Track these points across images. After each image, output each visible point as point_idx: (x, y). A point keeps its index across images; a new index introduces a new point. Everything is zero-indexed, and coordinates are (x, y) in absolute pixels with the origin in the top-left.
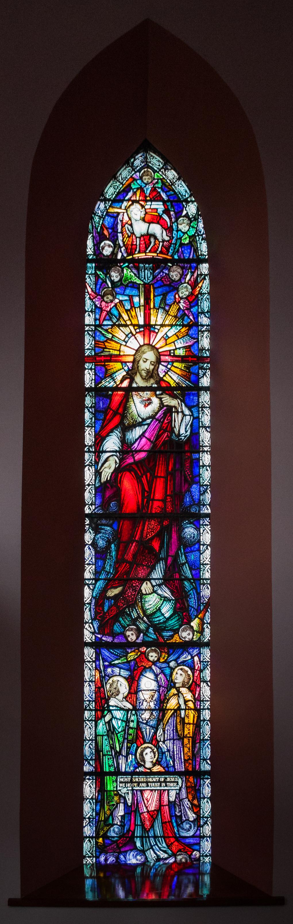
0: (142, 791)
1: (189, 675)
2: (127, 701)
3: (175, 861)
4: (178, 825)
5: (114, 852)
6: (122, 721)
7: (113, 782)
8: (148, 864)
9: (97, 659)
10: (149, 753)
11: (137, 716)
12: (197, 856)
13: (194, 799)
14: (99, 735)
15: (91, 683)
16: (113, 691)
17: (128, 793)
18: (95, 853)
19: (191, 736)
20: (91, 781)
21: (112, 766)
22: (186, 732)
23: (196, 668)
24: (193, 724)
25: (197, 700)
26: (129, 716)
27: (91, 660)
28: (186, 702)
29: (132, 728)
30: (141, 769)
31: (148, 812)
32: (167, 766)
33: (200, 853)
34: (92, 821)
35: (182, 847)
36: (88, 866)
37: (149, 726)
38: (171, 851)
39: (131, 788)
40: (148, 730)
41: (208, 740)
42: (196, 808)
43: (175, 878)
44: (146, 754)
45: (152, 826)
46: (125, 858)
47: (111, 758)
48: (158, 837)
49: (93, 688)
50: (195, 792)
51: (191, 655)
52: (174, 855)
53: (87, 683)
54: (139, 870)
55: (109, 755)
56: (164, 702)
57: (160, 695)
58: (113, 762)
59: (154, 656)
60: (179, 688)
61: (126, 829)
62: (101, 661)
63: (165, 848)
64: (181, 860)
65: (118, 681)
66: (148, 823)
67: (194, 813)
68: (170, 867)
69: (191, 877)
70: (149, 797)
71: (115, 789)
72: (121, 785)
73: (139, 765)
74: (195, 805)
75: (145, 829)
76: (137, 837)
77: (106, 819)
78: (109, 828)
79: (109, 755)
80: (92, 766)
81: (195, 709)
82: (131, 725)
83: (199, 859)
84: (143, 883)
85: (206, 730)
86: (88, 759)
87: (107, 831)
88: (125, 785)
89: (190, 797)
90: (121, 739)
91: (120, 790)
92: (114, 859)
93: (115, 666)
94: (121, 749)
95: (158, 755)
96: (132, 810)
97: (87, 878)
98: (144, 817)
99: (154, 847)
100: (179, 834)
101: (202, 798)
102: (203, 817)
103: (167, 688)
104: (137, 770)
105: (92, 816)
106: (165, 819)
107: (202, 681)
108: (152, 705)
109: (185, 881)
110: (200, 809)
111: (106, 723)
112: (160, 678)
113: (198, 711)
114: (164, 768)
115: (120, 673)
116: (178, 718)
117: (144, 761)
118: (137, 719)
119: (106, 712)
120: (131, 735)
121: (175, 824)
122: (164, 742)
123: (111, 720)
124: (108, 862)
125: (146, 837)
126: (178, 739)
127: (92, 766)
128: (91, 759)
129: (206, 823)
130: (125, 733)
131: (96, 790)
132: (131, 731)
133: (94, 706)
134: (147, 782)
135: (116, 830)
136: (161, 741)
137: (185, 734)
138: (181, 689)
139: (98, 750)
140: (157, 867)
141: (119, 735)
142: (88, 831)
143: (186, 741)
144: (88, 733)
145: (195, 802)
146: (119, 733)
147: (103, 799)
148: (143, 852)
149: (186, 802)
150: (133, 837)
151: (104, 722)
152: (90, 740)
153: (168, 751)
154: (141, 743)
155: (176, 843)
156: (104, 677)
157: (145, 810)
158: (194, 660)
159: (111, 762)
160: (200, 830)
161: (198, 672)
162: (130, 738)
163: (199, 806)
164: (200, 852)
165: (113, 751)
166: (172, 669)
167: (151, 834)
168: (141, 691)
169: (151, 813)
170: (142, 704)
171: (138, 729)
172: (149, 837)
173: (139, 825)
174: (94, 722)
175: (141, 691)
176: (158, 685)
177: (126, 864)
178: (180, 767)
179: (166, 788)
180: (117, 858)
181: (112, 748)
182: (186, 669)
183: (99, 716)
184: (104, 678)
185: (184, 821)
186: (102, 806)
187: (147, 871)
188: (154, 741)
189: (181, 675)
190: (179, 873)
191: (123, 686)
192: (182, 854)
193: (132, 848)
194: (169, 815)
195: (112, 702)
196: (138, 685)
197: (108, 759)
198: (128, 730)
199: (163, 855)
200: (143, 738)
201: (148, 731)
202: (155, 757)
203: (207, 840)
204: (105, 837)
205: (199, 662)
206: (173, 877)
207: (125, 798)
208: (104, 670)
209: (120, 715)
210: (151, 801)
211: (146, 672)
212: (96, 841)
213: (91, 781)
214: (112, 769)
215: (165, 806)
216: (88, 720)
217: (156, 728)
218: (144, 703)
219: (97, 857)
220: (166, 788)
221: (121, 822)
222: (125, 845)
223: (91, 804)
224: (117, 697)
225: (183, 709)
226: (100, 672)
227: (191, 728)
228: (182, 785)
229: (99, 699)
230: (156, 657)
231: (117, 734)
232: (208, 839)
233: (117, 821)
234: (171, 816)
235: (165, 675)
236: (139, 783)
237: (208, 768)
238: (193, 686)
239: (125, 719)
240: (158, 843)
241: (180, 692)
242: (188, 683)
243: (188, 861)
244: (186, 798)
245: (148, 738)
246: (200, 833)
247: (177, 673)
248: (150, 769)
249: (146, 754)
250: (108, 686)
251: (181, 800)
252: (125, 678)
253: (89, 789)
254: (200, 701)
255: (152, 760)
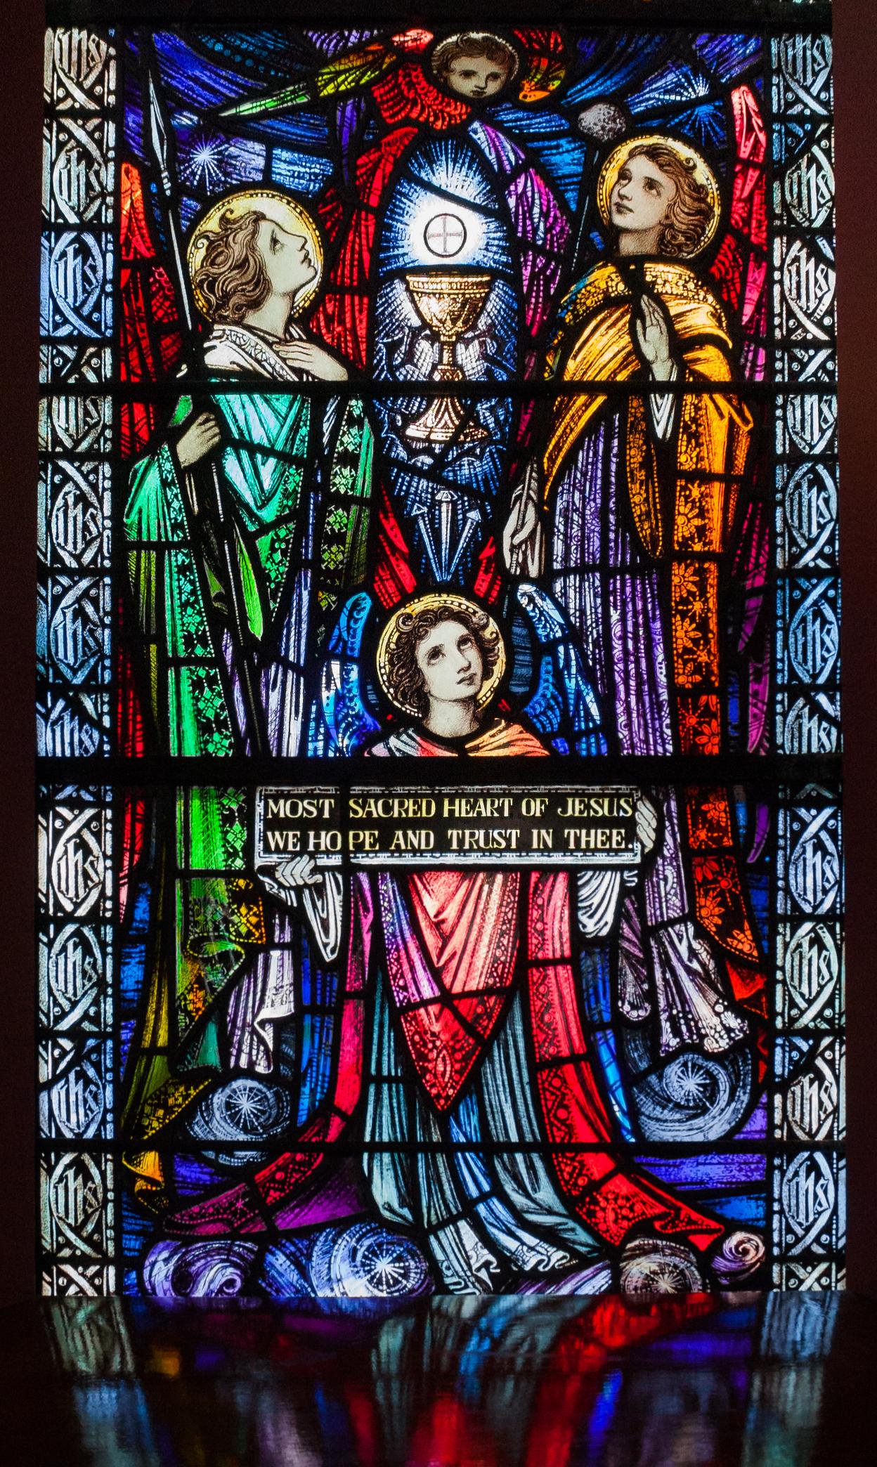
0: (406, 878)
1: (699, 190)
2: (314, 338)
3: (616, 1288)
4: (632, 1080)
5: (235, 1236)
6: (285, 458)
7: (228, 820)
8: (449, 1304)
9: (131, 96)
10: (450, 648)
11: (376, 428)
12: (751, 1258)
13: (731, 922)
14: (140, 545)
15: (89, 239)
16: (229, 279)
17: (319, 889)
18: (117, 1240)
19: (716, 546)
20: (89, 813)
21: (221, 725)
22: (684, 526)
23: (745, 151)
24: (726, 478)
25: (750, 333)
26: (327, 427)
27: (92, 106)
28: (681, 345)
29: (345, 502)
30: (403, 744)
31: (446, 999)
32: (566, 729)
33: (769, 1243)
34: (97, 1049)
35: (659, 1209)
36: (81, 1316)
37: (452, 485)
38: (588, 1229)
39: (336, 860)
40: (445, 512)
41: (818, 574)
42: (747, 979)
43: (608, 1392)
44: (436, 653)
45: (472, 1085)
46: (304, 1272)
47: (212, 681)
48: (511, 1148)
49: (106, 265)
50: (741, 890)
51: (713, 81)
52: (611, 1255)
53: (68, 237)
54: (391, 1340)
55: (200, 662)
56: (542, 349)
57: (523, 300)
58: (229, 704)
59: (483, 74)
60: (640, 260)
61: (305, 1102)
62: (155, 109)
63: (550, 1212)
64: (650, 1279)
65: (259, 217)
66: (442, 1066)
67: (735, 1007)
68: (577, 1324)
69: (704, 1383)
70: (450, 913)
71: (239, 863)
72: (275, 839)
73: (392, 722)
74: (739, 961)
75: (429, 1102)
76: (377, 1148)
77: (182, 1047)
78: (205, 1096)
79: (200, 662)
80: (97, 724)
81: (738, 389)
82: (342, 480)
83: (761, 1278)
84: (420, 1413)
85: (814, 514)
86: (67, 684)
87: (189, 1114)
88: (304, 841)
89: (711, 913)
90: (276, 568)
91: (269, 871)
92: (230, 1272)
93: (243, 129)
94: (275, 626)
95: (510, 664)
96: (345, 989)
97: (85, 1382)
98: (422, 1031)
99: (481, 1209)
100: (637, 1130)
101: (784, 919)
102: (788, 1032)
103: (564, 260)
104: (379, 750)
105: (95, 1020)
106: (554, 1040)
107: (780, 232)
108: (471, 360)
109: (668, 1405)
110: (772, 982)
111: (181, 472)
112: (521, 198)
113: (757, 399)
114: (545, 739)
115: (267, 171)
116: (636, 440)
117: (423, 699)
118: (379, 443)
119: (183, 408)
120: (338, 538)
121: (612, 1074)
122: (544, 584)
123: (214, 457)
124: (200, 1292)
125: (430, 1149)
126: (634, 570)
127: (97, 724)
128: (91, 686)
129: (805, 1066)
130: (300, 532)
131: (117, 869)
132: (337, 519)
133: (108, 372)
134: (439, 825)
135: (246, 1105)
136: (525, 578)
137: (678, 537)
138: (654, 271)
139: (134, 626)
140: (498, 1327)
141: (263, 543)
142: (68, 1107)
143: (682, 578)
144: (66, 524)
145: (743, 942)
146: (264, 529)
147: (161, 926)
148: (414, 1236)
149: (684, 942)
150: (352, 1146)
151: (168, 466)
152: (82, 572)
153: (574, 635)
154: (401, 588)
155: (621, 1185)
156: (172, 203)
157: (428, 991)
158: (729, 106)
159: (212, 704)
160: (770, 1108)
161: (753, 174)
162: (333, 557)
163: (767, 965)
164: (765, 1233)
165: (226, 638)
166: (597, 151)
167: (466, 1128)
168: (402, 273)
169: (463, 1006)
170: (410, 357)
171: (385, 499)
172: (450, 1148)
173: (390, 1080)
174: (106, 469)
175: (402, 273)
176: (510, 235)
177: (307, 1306)
178: (643, 734)
179: (558, 859)
180: (254, 1270)
181: (224, 616)
182: (684, 151)
183: (144, 434)
184: (174, 206)
185: (672, 1057)
186: (160, 966)
187: (438, 1346)
188: (485, 579)
189: (651, 184)
190: (634, 1360)
191: (291, 245)
192: (655, 1249)
193: (343, 1213)
194: (580, 1033)
195: (222, 354)
196: (384, 238)
197: (197, 685)
198: (322, 513)
199: (534, 1254)
200: (416, 555)
201: (445, 519)
202: (487, 674)
203: (813, 1167)
204: (177, 1143)
205: (757, 122)
206: (593, 1381)
207: (298, 918)
208: (172, 160)
209: (273, 424)
210: (466, 927)
211: (431, 162)
212: (119, 1171)
213: (89, 813)
214: (220, 746)
215: (555, 962)
216: (70, 456)
217: (496, 505)
218: (424, 345)
219: (129, 1263)
220: (558, 859)
221: (275, 1057)
222: (301, 1195)
223: (88, 951)
224: (251, 319)
225: (663, 388)
226: (149, 175)
227: (715, 504)
228: (659, 842)
229: (142, 329)
230: (494, 76)
231: (250, 539)
232: (819, 1157)
233: (252, 1054)
234: (589, 1028)
235: (553, 182)
236: (386, 831)
237: (820, 738)
238: (730, 257)
239: (300, 448)
240: (509, 1187)
241: (649, 289)
242: (694, 236)
243: (697, 1288)
244: (682, 920)
245: (443, 560)
246: (771, 1126)
247: (624, 175)
248: (455, 743)
249: (436, 653)
250: (197, 256)
251: (650, 932)
252: (296, 197)
253: (71, 861)
254: (771, 345)
255: (470, 691)
